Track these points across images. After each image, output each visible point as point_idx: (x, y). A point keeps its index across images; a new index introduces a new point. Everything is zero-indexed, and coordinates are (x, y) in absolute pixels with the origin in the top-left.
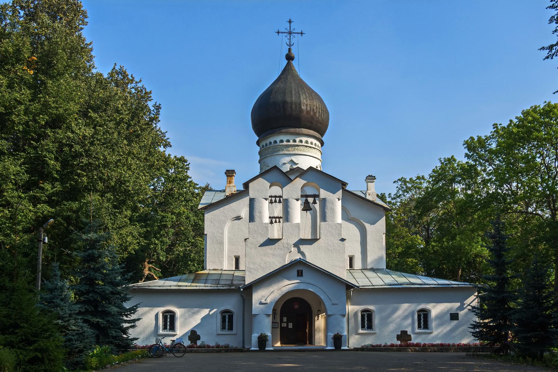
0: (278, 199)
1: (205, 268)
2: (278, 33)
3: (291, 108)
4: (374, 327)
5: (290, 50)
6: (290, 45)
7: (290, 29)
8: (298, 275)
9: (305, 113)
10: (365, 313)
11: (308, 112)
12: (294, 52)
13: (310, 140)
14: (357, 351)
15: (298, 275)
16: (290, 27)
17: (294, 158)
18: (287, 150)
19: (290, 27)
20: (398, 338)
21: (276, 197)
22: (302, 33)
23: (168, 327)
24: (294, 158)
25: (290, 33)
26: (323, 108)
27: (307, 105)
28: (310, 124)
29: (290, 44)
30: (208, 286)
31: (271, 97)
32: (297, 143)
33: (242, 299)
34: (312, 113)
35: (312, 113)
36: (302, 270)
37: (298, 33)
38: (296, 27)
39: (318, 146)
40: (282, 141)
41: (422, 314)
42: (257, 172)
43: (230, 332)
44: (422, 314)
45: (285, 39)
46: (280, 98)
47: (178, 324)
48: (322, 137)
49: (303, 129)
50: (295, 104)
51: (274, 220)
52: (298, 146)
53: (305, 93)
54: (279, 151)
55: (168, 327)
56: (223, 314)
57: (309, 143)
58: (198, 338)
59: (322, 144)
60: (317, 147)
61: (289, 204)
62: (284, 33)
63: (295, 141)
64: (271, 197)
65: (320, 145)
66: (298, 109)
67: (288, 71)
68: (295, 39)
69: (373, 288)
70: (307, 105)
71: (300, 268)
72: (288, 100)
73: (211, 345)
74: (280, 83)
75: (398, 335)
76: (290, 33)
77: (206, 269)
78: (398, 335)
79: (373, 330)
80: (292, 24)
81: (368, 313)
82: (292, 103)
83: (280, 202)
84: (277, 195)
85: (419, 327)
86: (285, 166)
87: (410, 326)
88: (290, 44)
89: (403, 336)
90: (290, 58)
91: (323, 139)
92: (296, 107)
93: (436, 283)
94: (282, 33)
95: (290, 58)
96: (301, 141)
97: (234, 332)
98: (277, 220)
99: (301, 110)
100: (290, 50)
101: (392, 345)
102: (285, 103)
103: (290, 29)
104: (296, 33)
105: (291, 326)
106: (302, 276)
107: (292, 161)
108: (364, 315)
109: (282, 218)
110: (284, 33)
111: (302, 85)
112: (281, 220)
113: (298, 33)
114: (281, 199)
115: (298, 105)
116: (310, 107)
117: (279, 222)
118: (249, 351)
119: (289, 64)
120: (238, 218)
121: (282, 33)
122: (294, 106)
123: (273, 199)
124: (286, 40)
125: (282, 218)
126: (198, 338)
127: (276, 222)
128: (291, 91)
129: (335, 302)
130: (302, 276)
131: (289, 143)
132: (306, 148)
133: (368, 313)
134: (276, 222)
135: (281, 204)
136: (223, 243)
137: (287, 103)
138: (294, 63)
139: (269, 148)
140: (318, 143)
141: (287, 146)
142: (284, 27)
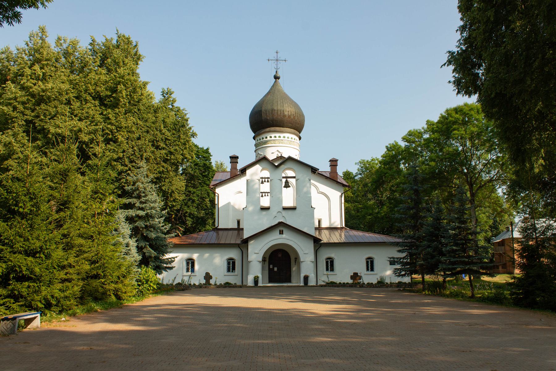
0: (266, 180)
2: (269, 60)
3: (277, 113)
4: (335, 270)
8: (280, 234)
9: (287, 117)
10: (328, 260)
11: (289, 117)
14: (321, 286)
15: (280, 234)
16: (277, 56)
19: (277, 56)
20: (352, 277)
21: (265, 178)
22: (285, 61)
23: (329, 269)
25: (277, 60)
26: (300, 113)
30: (188, 243)
33: (317, 251)
35: (292, 117)
36: (283, 230)
38: (281, 56)
39: (295, 139)
40: (284, 137)
41: (369, 260)
42: (253, 160)
43: (233, 274)
44: (369, 260)
45: (273, 64)
46: (269, 107)
47: (196, 267)
48: (300, 133)
50: (280, 111)
51: (264, 194)
52: (274, 140)
53: (287, 103)
55: (329, 269)
56: (327, 260)
58: (211, 277)
59: (300, 138)
62: (273, 60)
64: (262, 178)
65: (298, 139)
66: (282, 114)
68: (281, 64)
70: (288, 112)
71: (281, 229)
72: (276, 108)
73: (349, 283)
74: (269, 96)
75: (351, 276)
76: (277, 60)
78: (351, 276)
82: (278, 110)
83: (268, 181)
84: (264, 177)
87: (361, 269)
89: (355, 276)
91: (301, 135)
92: (281, 113)
94: (271, 60)
96: (275, 137)
97: (236, 273)
99: (284, 116)
101: (348, 283)
102: (273, 110)
103: (277, 58)
104: (281, 60)
105: (276, 269)
106: (283, 234)
108: (230, 262)
109: (269, 193)
110: (273, 60)
111: (286, 98)
112: (269, 194)
114: (269, 179)
115: (282, 112)
117: (268, 196)
118: (246, 286)
121: (271, 60)
122: (279, 112)
123: (264, 180)
125: (269, 193)
126: (211, 277)
127: (265, 196)
128: (277, 102)
129: (306, 252)
130: (283, 234)
134: (265, 196)
135: (269, 183)
142: (273, 56)
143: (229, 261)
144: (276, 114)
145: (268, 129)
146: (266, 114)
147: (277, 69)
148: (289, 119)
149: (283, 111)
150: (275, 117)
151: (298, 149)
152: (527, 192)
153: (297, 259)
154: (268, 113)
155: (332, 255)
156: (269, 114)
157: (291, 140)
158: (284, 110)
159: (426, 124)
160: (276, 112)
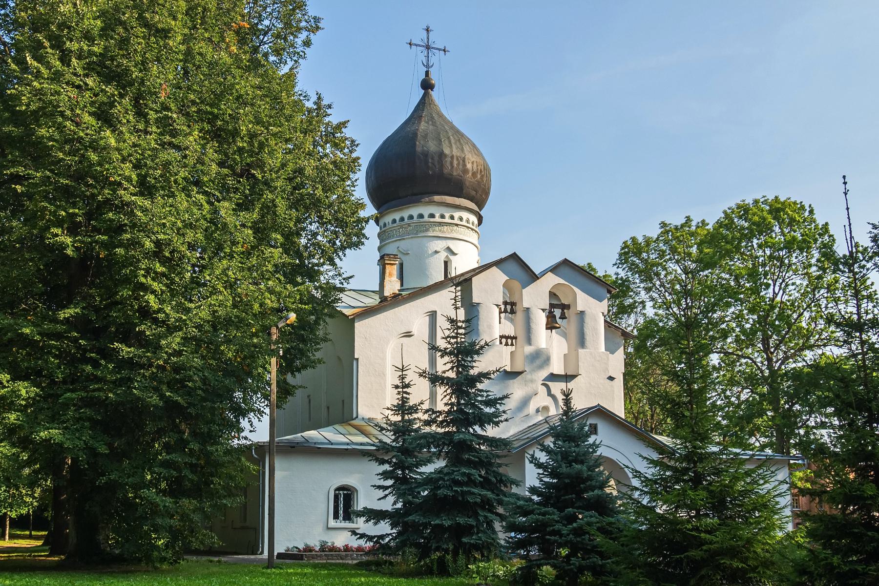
1: (355, 416)
5: (427, 73)
6: (427, 66)
7: (428, 42)
12: (434, 78)
13: (465, 215)
16: (428, 38)
17: (452, 245)
18: (440, 231)
19: (428, 38)
22: (444, 50)
24: (452, 245)
27: (473, 163)
28: (473, 193)
29: (428, 64)
31: (418, 143)
32: (456, 221)
34: (479, 176)
37: (440, 50)
38: (437, 40)
39: (468, 221)
40: (432, 216)
49: (446, 197)
52: (457, 225)
54: (427, 230)
57: (464, 220)
60: (471, 226)
61: (532, 316)
62: (419, 46)
63: (442, 216)
65: (476, 222)
67: (424, 103)
69: (347, 449)
77: (357, 417)
79: (353, 523)
80: (431, 34)
81: (345, 492)
85: (336, 517)
86: (437, 255)
88: (428, 64)
90: (427, 85)
91: (481, 213)
93: (345, 440)
94: (416, 45)
95: (427, 85)
98: (509, 341)
100: (427, 73)
103: (428, 42)
107: (449, 249)
110: (419, 46)
113: (440, 50)
116: (477, 166)
119: (425, 96)
120: (408, 335)
121: (416, 45)
124: (422, 57)
131: (443, 220)
132: (455, 227)
133: (345, 492)
136: (384, 375)
137: (446, 156)
138: (434, 94)
139: (409, 225)
140: (474, 219)
141: (441, 224)
142: (419, 37)
143: (337, 492)
144: (448, 164)
145: (437, 198)
146: (427, 162)
147: (427, 66)
148: (473, 180)
149: (464, 161)
150: (445, 171)
151: (476, 243)
152: (316, 268)
153: (357, 491)
154: (430, 161)
155: (351, 481)
156: (433, 163)
157: (459, 222)
158: (464, 158)
159: (321, 109)
160: (448, 159)
